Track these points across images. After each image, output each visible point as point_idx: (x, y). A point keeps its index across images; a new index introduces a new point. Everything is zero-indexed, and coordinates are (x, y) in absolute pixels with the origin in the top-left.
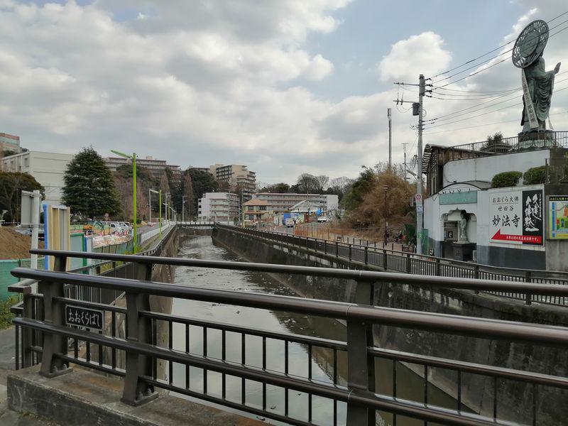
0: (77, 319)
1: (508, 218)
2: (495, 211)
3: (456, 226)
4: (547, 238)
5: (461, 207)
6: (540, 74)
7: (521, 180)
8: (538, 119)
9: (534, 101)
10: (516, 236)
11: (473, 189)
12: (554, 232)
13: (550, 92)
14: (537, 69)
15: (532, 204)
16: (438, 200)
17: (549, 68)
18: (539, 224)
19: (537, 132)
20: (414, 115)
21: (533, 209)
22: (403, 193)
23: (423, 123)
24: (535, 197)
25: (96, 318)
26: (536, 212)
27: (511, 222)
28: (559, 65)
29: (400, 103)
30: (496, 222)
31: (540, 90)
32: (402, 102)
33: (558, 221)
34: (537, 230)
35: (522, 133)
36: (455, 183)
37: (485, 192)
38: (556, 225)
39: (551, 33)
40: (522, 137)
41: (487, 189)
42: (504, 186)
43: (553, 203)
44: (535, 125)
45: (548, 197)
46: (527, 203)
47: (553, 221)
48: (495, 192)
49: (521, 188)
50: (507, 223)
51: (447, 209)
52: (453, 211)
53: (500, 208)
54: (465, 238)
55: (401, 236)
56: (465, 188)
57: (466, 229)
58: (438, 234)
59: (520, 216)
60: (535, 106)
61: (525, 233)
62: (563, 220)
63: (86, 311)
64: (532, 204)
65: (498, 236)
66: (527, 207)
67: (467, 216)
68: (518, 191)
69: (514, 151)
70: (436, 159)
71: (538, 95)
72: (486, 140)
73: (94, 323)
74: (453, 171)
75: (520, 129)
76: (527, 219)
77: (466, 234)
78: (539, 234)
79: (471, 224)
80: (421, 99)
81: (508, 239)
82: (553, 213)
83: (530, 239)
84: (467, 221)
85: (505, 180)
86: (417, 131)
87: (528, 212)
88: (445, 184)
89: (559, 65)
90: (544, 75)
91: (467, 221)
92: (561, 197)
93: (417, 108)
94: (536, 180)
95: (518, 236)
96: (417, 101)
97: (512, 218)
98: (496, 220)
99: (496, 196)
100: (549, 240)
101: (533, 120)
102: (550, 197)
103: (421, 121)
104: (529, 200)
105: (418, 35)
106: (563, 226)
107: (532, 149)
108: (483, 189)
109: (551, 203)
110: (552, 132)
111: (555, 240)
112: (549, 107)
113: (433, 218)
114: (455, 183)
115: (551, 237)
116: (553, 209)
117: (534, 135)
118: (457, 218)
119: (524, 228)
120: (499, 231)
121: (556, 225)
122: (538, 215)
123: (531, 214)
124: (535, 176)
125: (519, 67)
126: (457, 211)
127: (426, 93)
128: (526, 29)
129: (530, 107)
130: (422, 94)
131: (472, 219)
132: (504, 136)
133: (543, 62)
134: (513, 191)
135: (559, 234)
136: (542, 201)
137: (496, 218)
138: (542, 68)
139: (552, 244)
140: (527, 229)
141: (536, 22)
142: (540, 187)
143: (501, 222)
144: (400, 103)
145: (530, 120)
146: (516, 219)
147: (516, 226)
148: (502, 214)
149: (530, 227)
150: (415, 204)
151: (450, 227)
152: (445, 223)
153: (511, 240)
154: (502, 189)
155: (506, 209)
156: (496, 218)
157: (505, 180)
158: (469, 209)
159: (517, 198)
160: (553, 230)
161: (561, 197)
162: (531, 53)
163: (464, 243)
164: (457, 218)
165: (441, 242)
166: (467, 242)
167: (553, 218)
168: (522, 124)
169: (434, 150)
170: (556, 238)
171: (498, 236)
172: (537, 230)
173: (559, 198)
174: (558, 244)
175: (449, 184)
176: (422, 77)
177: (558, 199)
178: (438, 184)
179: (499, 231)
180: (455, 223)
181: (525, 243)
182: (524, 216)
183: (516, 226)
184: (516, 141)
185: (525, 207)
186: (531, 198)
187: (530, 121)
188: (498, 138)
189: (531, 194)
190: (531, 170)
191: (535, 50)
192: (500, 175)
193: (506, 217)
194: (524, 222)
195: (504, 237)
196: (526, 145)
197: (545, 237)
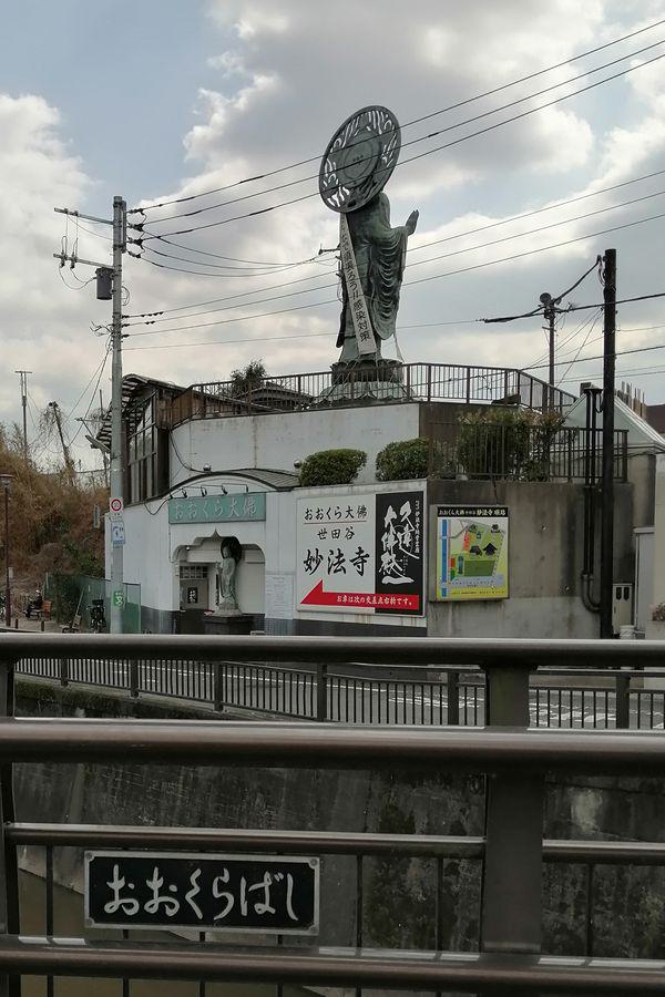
0: (157, 900)
1: (341, 555)
2: (310, 541)
3: (205, 576)
4: (430, 599)
5: (226, 531)
6: (381, 233)
7: (369, 469)
8: (375, 333)
9: (367, 293)
10: (360, 595)
11: (255, 487)
12: (445, 585)
13: (400, 278)
14: (375, 219)
15: (399, 524)
16: (164, 513)
17: (397, 221)
18: (414, 568)
19: (373, 362)
20: (615, 250)
21: (399, 535)
22: (29, 498)
23: (124, 321)
24: (406, 509)
25: (278, 889)
26: (407, 541)
27: (347, 565)
28: (415, 216)
29: (68, 263)
30: (314, 565)
31: (381, 268)
32: (74, 260)
33: (453, 561)
34: (410, 580)
35: (341, 364)
36: (208, 473)
37: (284, 495)
38: (448, 568)
39: (406, 135)
40: (340, 373)
41: (290, 489)
42: (329, 483)
43: (445, 522)
44: (366, 347)
45: (434, 508)
46: (387, 520)
47: (444, 561)
48: (320, 496)
49: (371, 488)
50: (338, 564)
51: (188, 535)
52: (205, 540)
53: (322, 533)
54: (232, 601)
55: (39, 603)
56: (236, 486)
57: (233, 581)
58: (164, 595)
59: (370, 549)
60: (370, 303)
61: (382, 589)
62: (461, 559)
63: (212, 869)
64: (399, 524)
65: (317, 596)
66: (388, 530)
67: (233, 548)
68: (363, 493)
69: (315, 408)
70: (148, 413)
71: (377, 280)
72: (228, 378)
73: (263, 908)
74: (197, 445)
75: (335, 354)
76: (385, 558)
77: (234, 595)
78: (414, 589)
79: (247, 571)
80: (117, 259)
81: (342, 604)
82: (444, 541)
83: (393, 601)
84: (237, 562)
85: (331, 469)
86: (107, 337)
87: (389, 540)
88: (178, 474)
89: (415, 216)
90: (389, 235)
91: (237, 562)
92: (460, 509)
93: (107, 282)
94: (408, 469)
95: (365, 596)
96: (109, 262)
97: (350, 554)
98: (312, 561)
99: (314, 505)
100: (435, 603)
101: (365, 336)
102: (439, 509)
103: (117, 315)
104: (391, 514)
105: (15, 97)
106: (460, 572)
107: (366, 401)
108: (280, 489)
109: (440, 520)
110: (401, 365)
111: (446, 603)
112: (396, 308)
113: (145, 560)
114: (208, 473)
115: (440, 596)
116: (444, 533)
117: (363, 375)
118: (212, 555)
119: (379, 577)
120: (320, 585)
121: (448, 568)
122: (411, 548)
123: (396, 546)
124: (399, 463)
125: (335, 208)
126: (216, 538)
127: (130, 247)
128: (349, 121)
129: (358, 304)
130: (119, 247)
131: (249, 557)
132: (269, 372)
133: (386, 204)
134: (353, 494)
135: (453, 591)
136: (421, 516)
137: (313, 554)
138: (386, 220)
139: (440, 609)
140: (386, 580)
141: (373, 109)
142: (418, 485)
143: (324, 564)
144: (68, 263)
145: (358, 334)
146: (361, 557)
147: (361, 573)
148: (326, 547)
149: (394, 575)
150: (103, 524)
151: (194, 576)
152: (181, 568)
153: (348, 604)
154: (327, 490)
155: (336, 534)
156: (313, 554)
157: (331, 469)
158: (244, 535)
159: (363, 511)
160: (444, 580)
161: (460, 509)
162: (362, 180)
163: (231, 613)
164: (212, 555)
165: (174, 613)
166: (237, 613)
167: (444, 555)
168: (338, 346)
169: (137, 393)
170: (451, 596)
171: (317, 596)
172: (410, 580)
173: (455, 509)
174: (451, 608)
175: (194, 474)
176: (119, 204)
177: (453, 512)
178: (151, 477)
179: (320, 585)
180: (204, 569)
181: (381, 610)
182: (380, 551)
183: (361, 573)
184: (326, 382)
185: (381, 530)
186: (397, 510)
187: (358, 337)
188: (255, 374)
189: (395, 500)
190: (312, 459)
191: (371, 176)
192: (321, 456)
193: (336, 554)
194: (379, 563)
195: (331, 599)
196: (344, 390)
197: (427, 597)
